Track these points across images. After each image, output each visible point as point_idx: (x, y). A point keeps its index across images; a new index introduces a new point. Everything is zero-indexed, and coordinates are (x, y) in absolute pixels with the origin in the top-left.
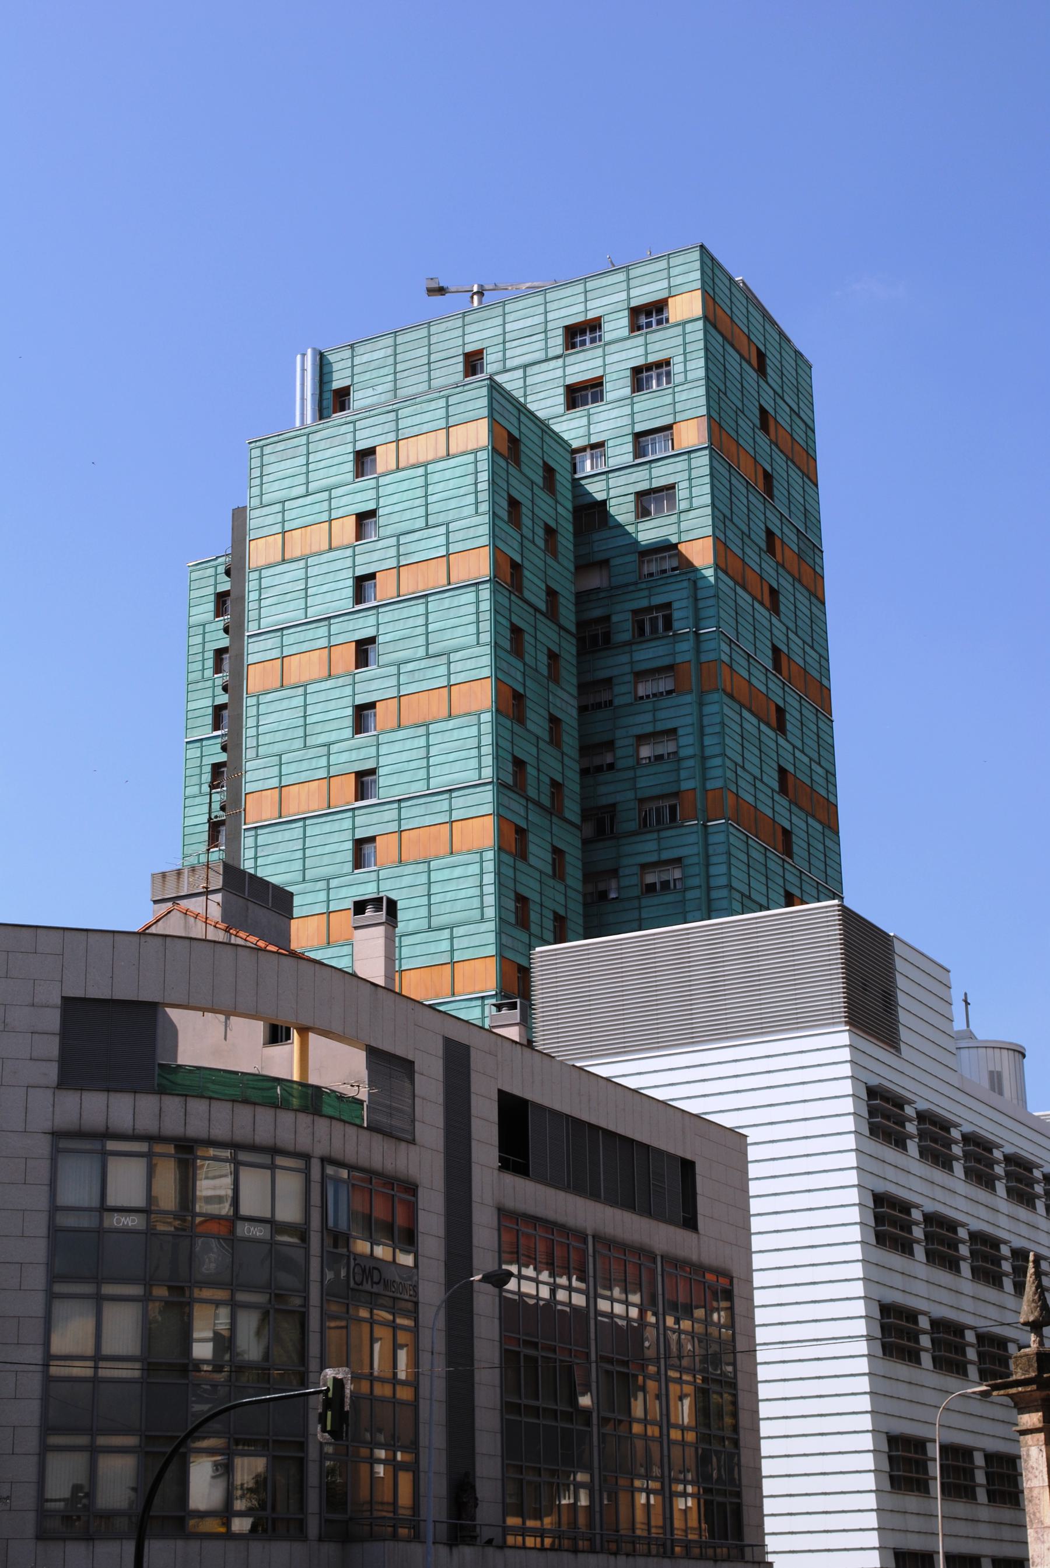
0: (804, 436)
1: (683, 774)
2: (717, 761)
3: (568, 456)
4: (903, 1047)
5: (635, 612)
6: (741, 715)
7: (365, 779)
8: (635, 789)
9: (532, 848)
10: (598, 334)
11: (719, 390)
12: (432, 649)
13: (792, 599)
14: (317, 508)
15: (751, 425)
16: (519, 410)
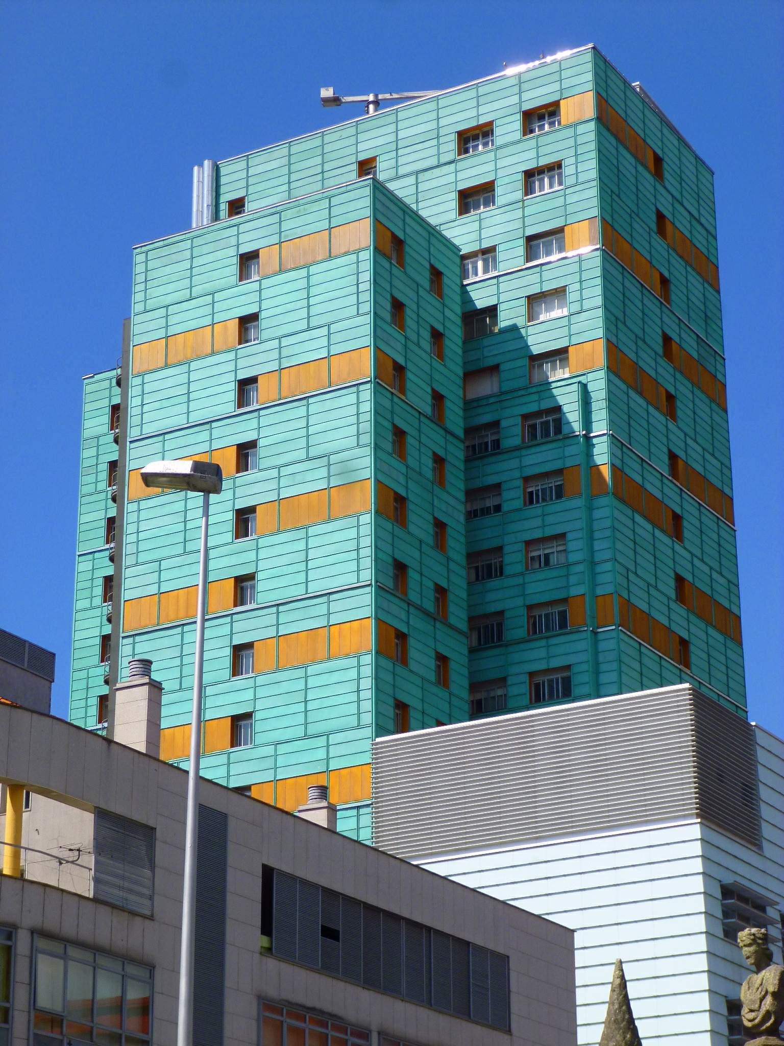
0: (705, 243)
1: (573, 579)
2: (608, 566)
3: (458, 261)
4: (765, 844)
5: (525, 417)
6: (633, 520)
7: (244, 584)
8: (524, 595)
9: (413, 654)
10: (490, 139)
11: (612, 191)
12: (313, 452)
13: (691, 406)
14: (201, 312)
15: (647, 229)
16: (404, 211)
